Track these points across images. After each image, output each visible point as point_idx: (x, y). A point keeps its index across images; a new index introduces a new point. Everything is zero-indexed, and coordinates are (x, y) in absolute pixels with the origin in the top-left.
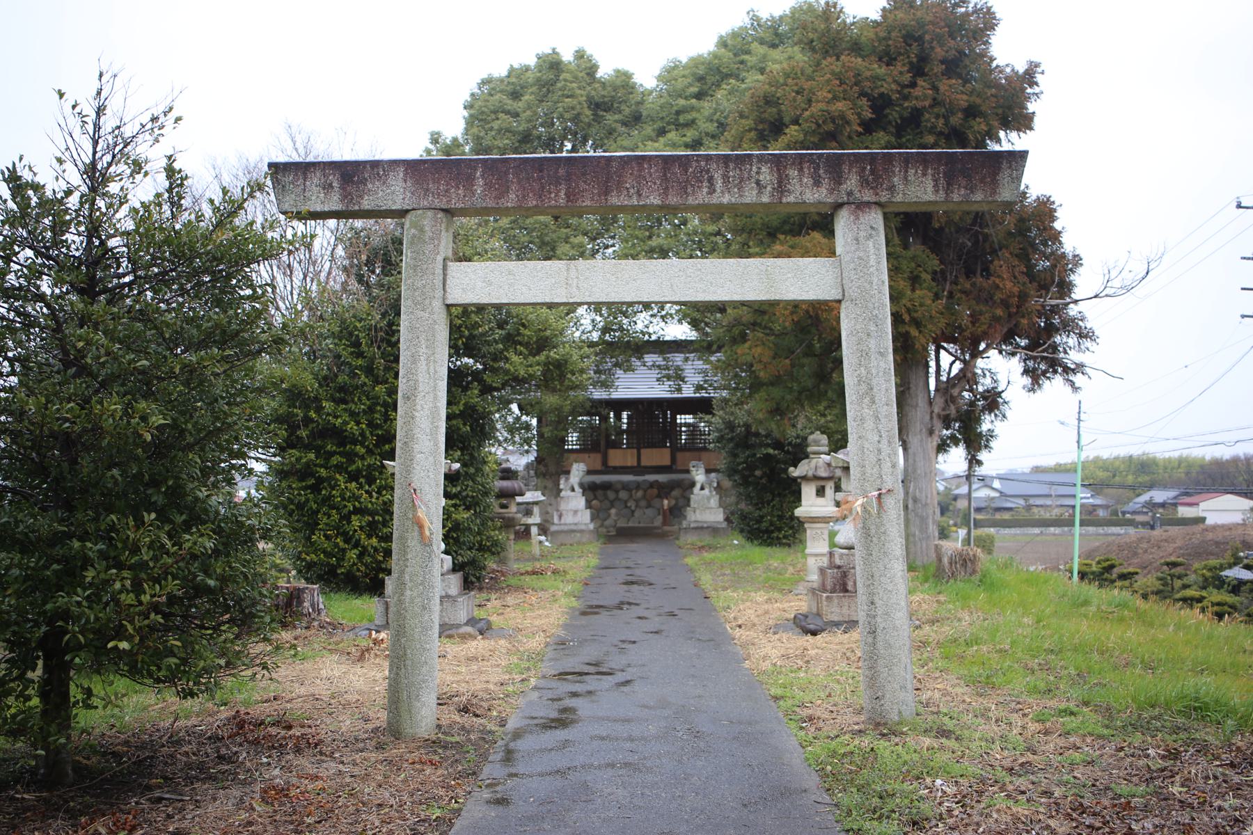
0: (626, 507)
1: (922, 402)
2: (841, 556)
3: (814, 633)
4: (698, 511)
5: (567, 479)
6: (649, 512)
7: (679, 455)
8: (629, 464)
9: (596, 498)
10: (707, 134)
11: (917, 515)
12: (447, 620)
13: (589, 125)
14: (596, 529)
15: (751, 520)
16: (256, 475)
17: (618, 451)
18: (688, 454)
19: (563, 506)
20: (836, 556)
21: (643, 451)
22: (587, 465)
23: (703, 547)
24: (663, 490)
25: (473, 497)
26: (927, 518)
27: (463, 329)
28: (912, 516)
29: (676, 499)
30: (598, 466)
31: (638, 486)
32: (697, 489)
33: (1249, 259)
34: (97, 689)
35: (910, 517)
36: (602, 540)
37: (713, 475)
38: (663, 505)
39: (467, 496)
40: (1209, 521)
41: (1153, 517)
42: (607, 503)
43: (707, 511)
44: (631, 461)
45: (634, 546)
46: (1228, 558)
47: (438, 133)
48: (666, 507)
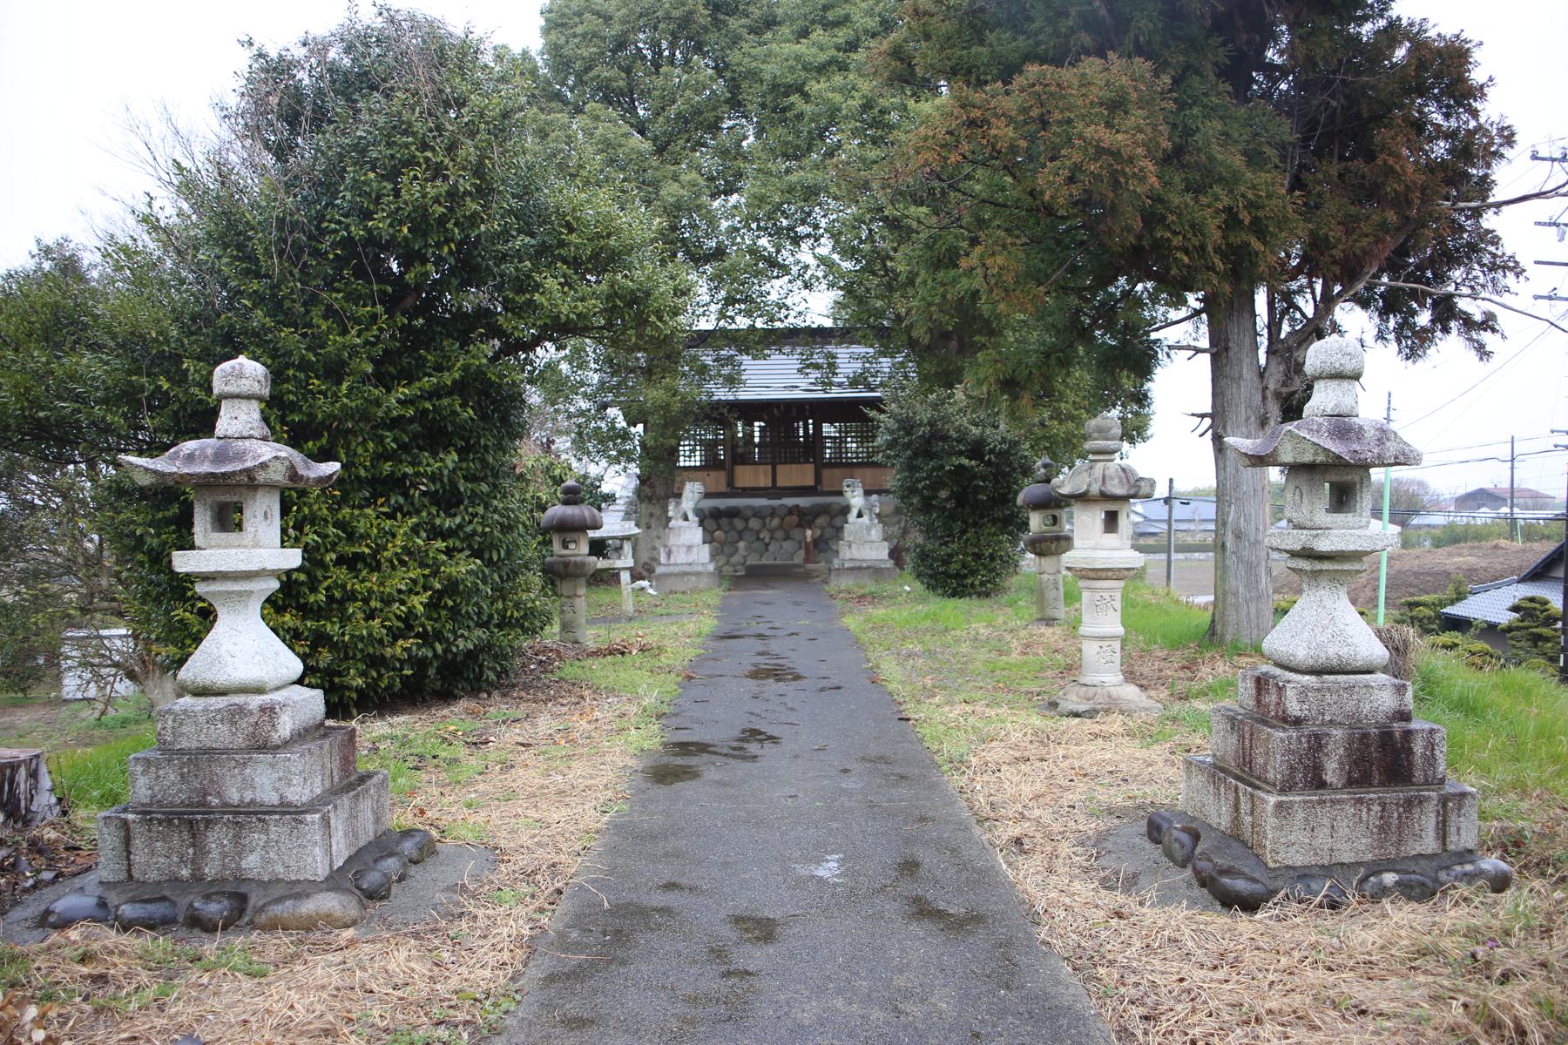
0: (758, 539)
1: (1248, 374)
2: (1304, 692)
3: (1250, 905)
4: (854, 546)
5: (678, 504)
6: (787, 545)
7: (826, 473)
8: (762, 485)
9: (719, 528)
10: (866, 32)
11: (1240, 559)
12: (280, 869)
13: (706, 29)
14: (719, 570)
15: (935, 560)
18: (837, 471)
19: (673, 540)
20: (1290, 693)
21: (779, 467)
22: (704, 485)
23: (862, 597)
24: (805, 518)
25: (484, 534)
26: (1258, 564)
27: (450, 226)
28: (1231, 561)
29: (822, 529)
30: (723, 488)
31: (773, 512)
32: (852, 516)
33: (1545, 224)
35: (1228, 562)
36: (726, 584)
37: (875, 497)
38: (805, 537)
39: (474, 533)
42: (734, 535)
43: (867, 546)
44: (764, 481)
45: (767, 593)
46: (1450, 592)
47: (504, 47)
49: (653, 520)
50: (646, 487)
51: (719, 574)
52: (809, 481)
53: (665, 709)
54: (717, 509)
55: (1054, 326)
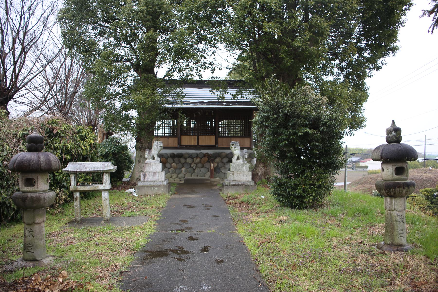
0: (191, 167)
4: (235, 174)
5: (150, 152)
6: (203, 170)
7: (220, 140)
8: (193, 144)
9: (174, 162)
16: (55, 149)
17: (187, 137)
19: (147, 169)
21: (200, 137)
24: (211, 158)
29: (218, 163)
30: (176, 145)
31: (197, 156)
32: (234, 160)
34: (267, 131)
36: (173, 189)
38: (211, 167)
40: (369, 169)
41: (353, 166)
42: (180, 165)
43: (241, 174)
48: (212, 168)
49: (141, 159)
50: (139, 143)
51: (170, 185)
52: (213, 143)
53: (237, 77)
54: (173, 154)
55: (66, 224)
